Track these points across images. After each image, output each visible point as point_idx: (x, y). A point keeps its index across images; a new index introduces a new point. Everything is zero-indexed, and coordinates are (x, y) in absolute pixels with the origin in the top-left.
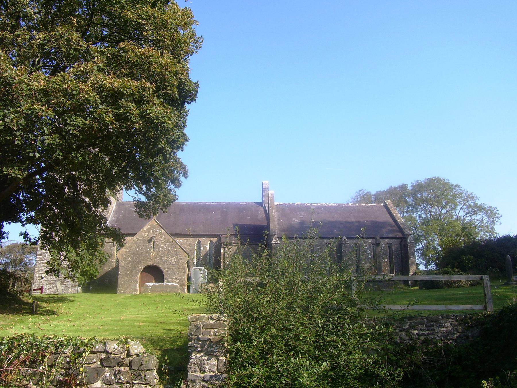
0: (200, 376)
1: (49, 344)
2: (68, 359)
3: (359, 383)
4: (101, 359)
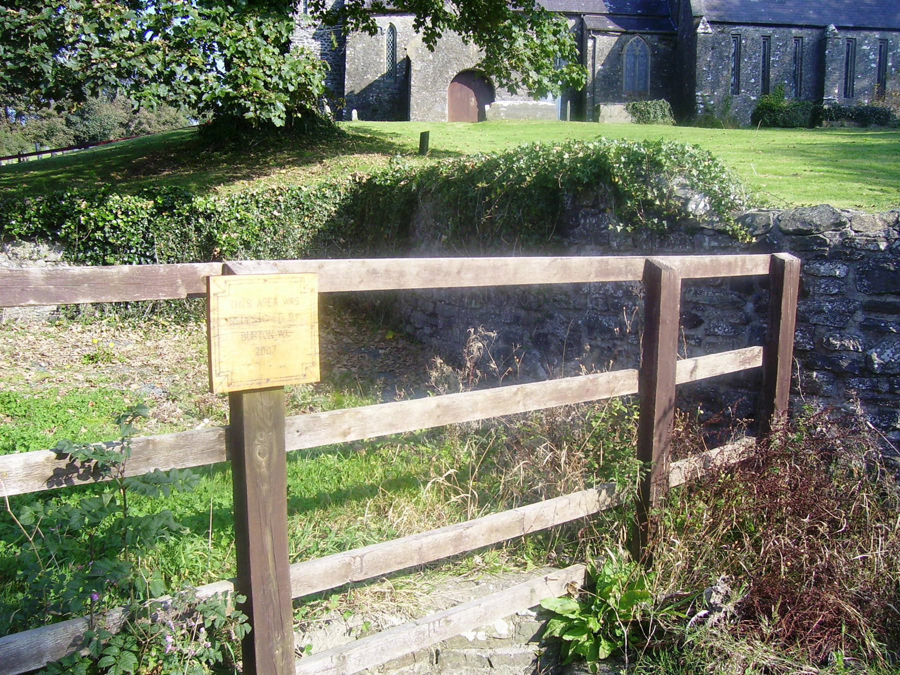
0: (155, 172)
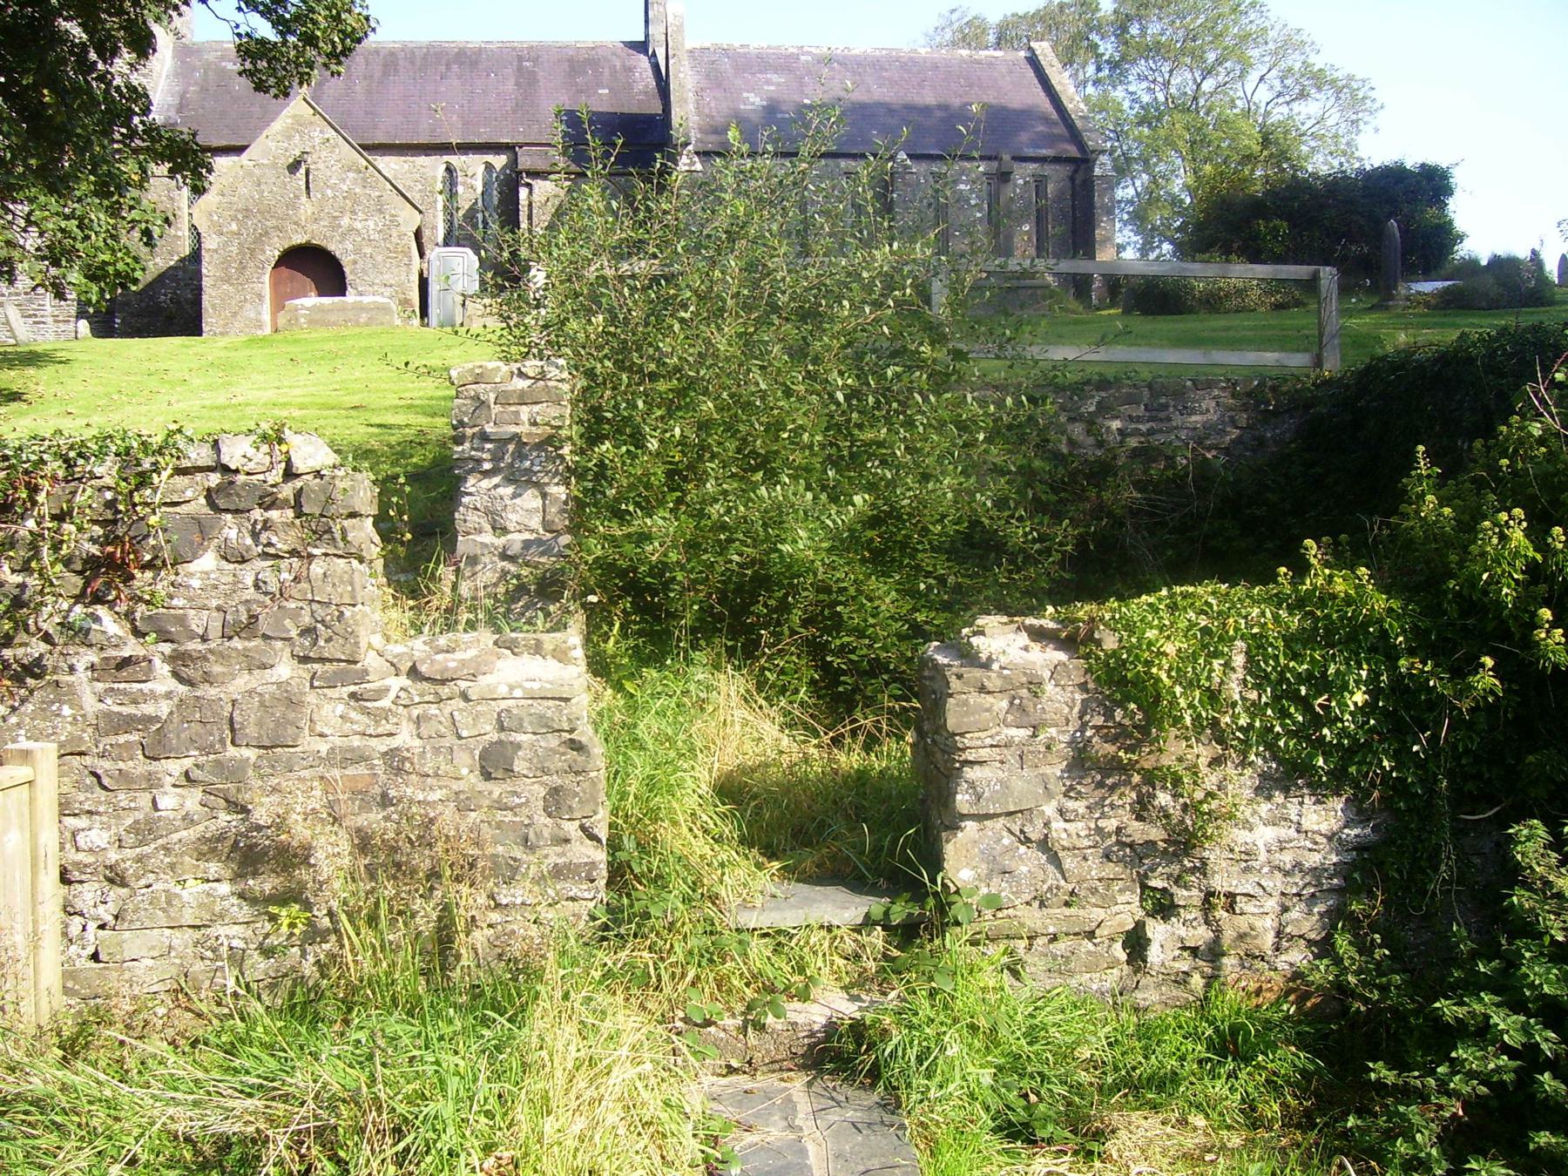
1: (44, 452)
2: (109, 495)
3: (950, 564)
4: (209, 490)
